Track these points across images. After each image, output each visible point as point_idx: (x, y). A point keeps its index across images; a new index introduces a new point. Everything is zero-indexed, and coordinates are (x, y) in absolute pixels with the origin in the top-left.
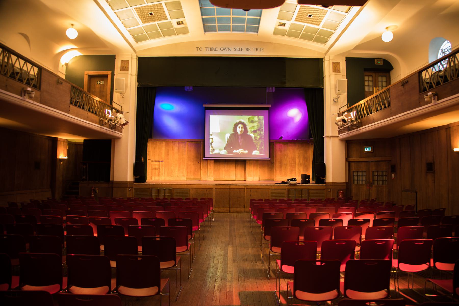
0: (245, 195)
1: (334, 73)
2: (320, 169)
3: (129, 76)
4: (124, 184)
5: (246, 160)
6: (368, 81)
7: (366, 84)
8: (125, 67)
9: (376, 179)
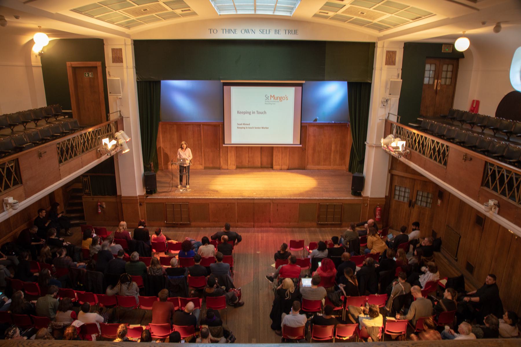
0: (271, 209)
1: (387, 66)
2: (358, 185)
3: (125, 70)
4: (132, 200)
5: (273, 147)
6: (429, 70)
7: (427, 74)
8: (118, 58)
9: (420, 199)
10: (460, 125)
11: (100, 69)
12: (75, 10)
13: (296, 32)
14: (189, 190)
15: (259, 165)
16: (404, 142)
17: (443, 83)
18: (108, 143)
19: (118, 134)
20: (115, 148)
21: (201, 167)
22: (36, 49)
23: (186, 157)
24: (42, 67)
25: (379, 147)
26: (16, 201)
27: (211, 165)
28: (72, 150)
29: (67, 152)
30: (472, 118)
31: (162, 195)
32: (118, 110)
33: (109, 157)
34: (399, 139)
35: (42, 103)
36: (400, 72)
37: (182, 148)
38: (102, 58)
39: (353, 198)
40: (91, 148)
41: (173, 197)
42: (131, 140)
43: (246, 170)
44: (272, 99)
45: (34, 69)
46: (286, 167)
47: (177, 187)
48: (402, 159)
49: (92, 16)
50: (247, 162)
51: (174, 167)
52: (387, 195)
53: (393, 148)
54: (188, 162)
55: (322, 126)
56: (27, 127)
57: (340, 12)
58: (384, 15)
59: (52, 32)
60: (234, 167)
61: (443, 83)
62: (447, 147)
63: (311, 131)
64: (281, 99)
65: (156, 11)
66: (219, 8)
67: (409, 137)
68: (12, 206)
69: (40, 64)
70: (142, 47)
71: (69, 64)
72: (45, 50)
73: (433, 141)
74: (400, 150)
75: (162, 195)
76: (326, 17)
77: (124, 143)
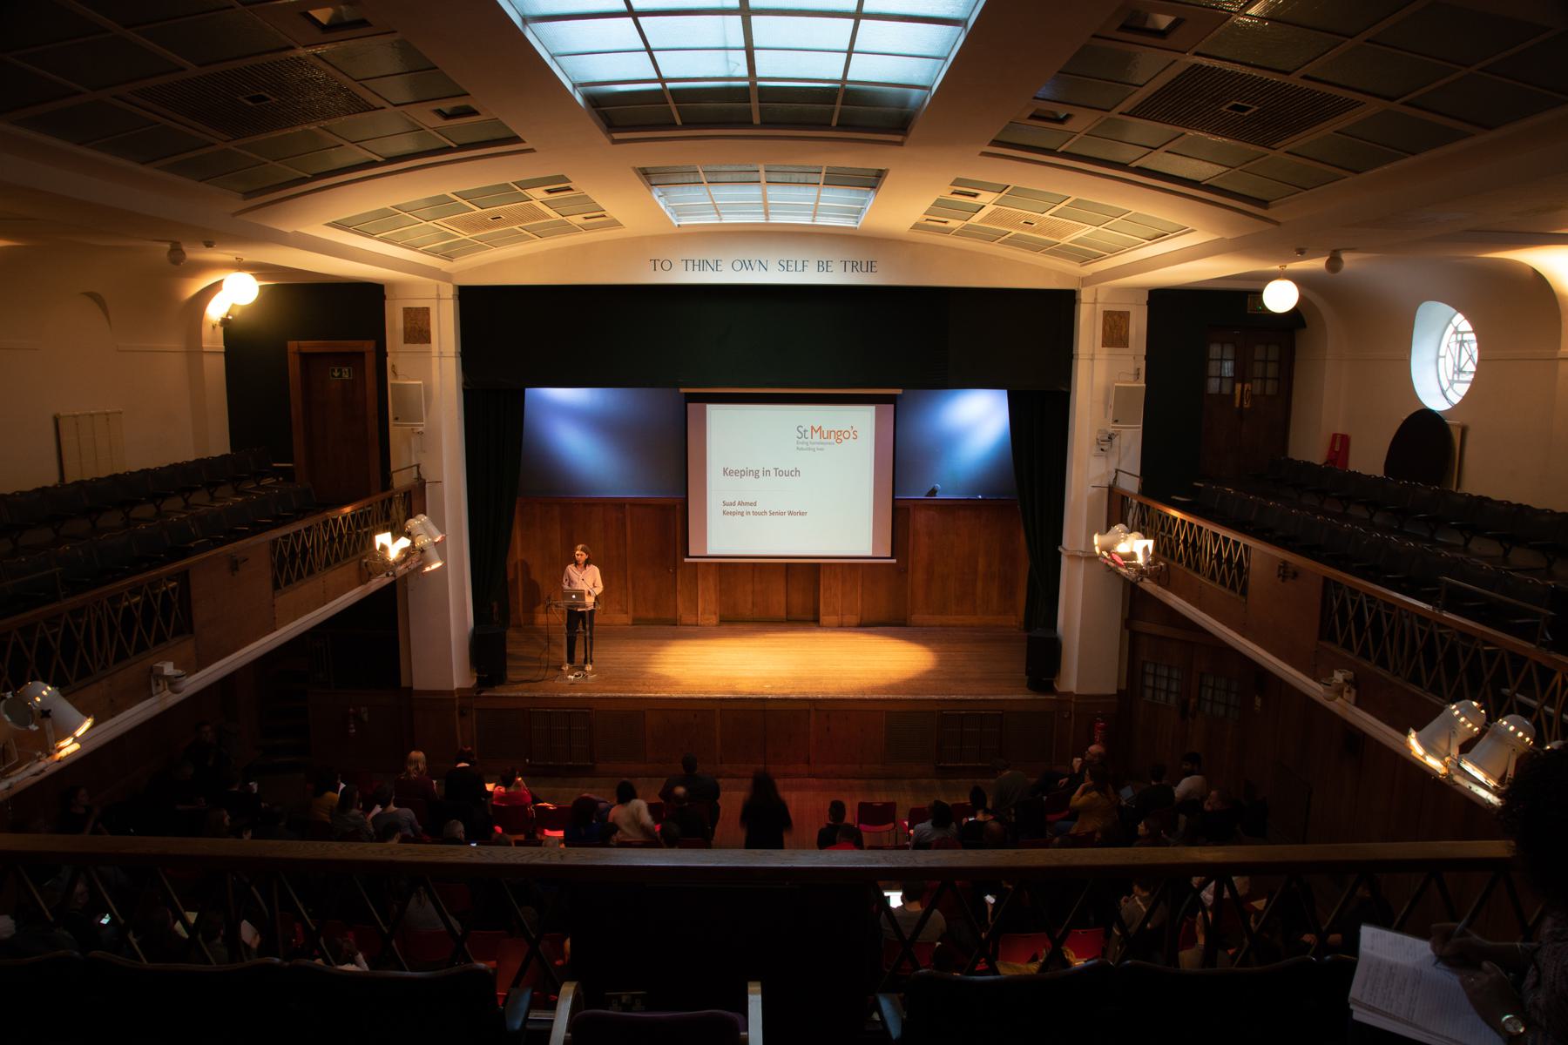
2: (1043, 656)
3: (435, 361)
4: (440, 701)
8: (418, 330)
9: (1209, 696)
10: (1366, 515)
11: (370, 361)
12: (338, 225)
13: (870, 266)
14: (591, 677)
15: (782, 614)
16: (1150, 543)
17: (1257, 391)
18: (390, 545)
19: (413, 523)
20: (405, 560)
21: (624, 619)
22: (216, 311)
23: (586, 589)
24: (226, 353)
25: (1091, 558)
26: (180, 672)
27: (652, 615)
28: (340, 542)
29: (293, 563)
30: (1333, 480)
31: (513, 691)
32: (414, 462)
33: (387, 581)
34: (1136, 534)
35: (219, 445)
36: (1142, 365)
37: (577, 564)
38: (376, 330)
39: (1027, 695)
40: (346, 556)
41: (549, 694)
42: (444, 539)
43: (746, 628)
44: (817, 436)
45: (206, 358)
46: (854, 619)
47: (559, 668)
48: (1148, 585)
49: (370, 235)
50: (749, 606)
51: (552, 619)
53: (1123, 557)
54: (590, 600)
55: (951, 508)
56: (191, 501)
57: (976, 219)
58: (1080, 228)
59: (260, 270)
60: (714, 619)
61: (1257, 391)
62: (1246, 547)
63: (921, 520)
64: (839, 436)
65: (522, 221)
66: (678, 212)
67: (1162, 529)
68: (172, 682)
69: (221, 346)
70: (483, 308)
71: (293, 345)
72: (237, 312)
73: (1216, 536)
74: (1140, 560)
75: (513, 691)
76: (947, 231)
77: (428, 545)
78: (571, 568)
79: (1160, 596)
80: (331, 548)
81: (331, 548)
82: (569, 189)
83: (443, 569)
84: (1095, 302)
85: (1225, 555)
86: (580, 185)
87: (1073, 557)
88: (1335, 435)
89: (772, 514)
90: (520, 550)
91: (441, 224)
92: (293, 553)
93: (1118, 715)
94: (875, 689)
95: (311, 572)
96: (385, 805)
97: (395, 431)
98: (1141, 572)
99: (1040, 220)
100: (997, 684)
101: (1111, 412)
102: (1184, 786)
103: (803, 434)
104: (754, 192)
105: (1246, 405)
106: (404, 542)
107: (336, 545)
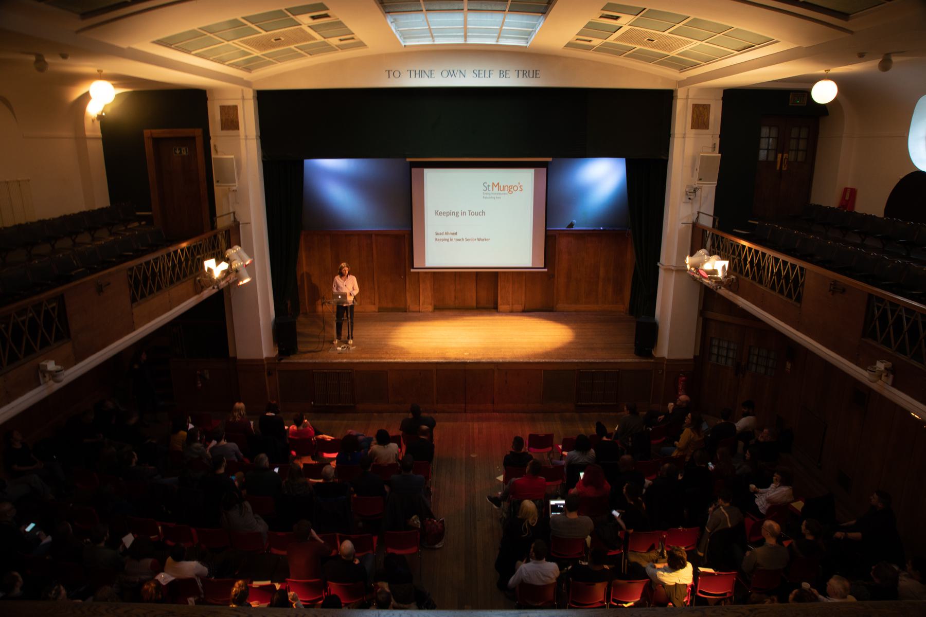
1: (694, 131)
2: (646, 334)
3: (243, 142)
4: (255, 365)
6: (767, 139)
7: (764, 143)
8: (230, 121)
11: (199, 142)
12: (160, 43)
13: (535, 74)
15: (474, 304)
16: (726, 263)
18: (215, 268)
19: (231, 252)
21: (372, 308)
22: (94, 109)
25: (682, 270)
26: (59, 367)
27: (391, 305)
30: (844, 218)
32: (231, 210)
35: (101, 199)
37: (342, 275)
40: (185, 276)
41: (325, 361)
42: (252, 263)
44: (496, 189)
46: (520, 308)
47: (332, 342)
48: (723, 291)
51: (327, 309)
52: (698, 354)
53: (708, 272)
54: (350, 299)
57: (612, 39)
58: (688, 42)
59: (119, 79)
60: (430, 308)
64: (510, 189)
66: (405, 36)
67: (734, 253)
68: (54, 375)
69: (99, 134)
70: (269, 101)
71: (147, 133)
72: (108, 110)
73: (777, 260)
74: (720, 275)
76: (588, 48)
77: (239, 267)
78: (338, 279)
79: (731, 299)
80: (173, 271)
81: (173, 271)
82: (326, 16)
83: (252, 284)
84: (687, 98)
85: (784, 273)
86: (337, 14)
87: (668, 270)
88: (846, 189)
89: (467, 240)
90: (306, 265)
91: (237, 44)
92: (146, 278)
93: (694, 373)
94: (536, 355)
95: (159, 288)
96: (219, 440)
97: (218, 189)
98: (719, 282)
99: (661, 37)
100: (618, 353)
101: (697, 174)
102: (742, 423)
103: (487, 188)
104: (458, 18)
105: (784, 169)
106: (224, 266)
107: (177, 269)
